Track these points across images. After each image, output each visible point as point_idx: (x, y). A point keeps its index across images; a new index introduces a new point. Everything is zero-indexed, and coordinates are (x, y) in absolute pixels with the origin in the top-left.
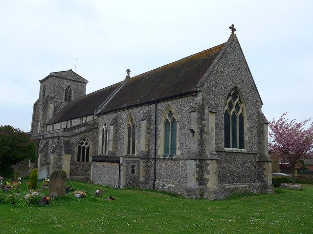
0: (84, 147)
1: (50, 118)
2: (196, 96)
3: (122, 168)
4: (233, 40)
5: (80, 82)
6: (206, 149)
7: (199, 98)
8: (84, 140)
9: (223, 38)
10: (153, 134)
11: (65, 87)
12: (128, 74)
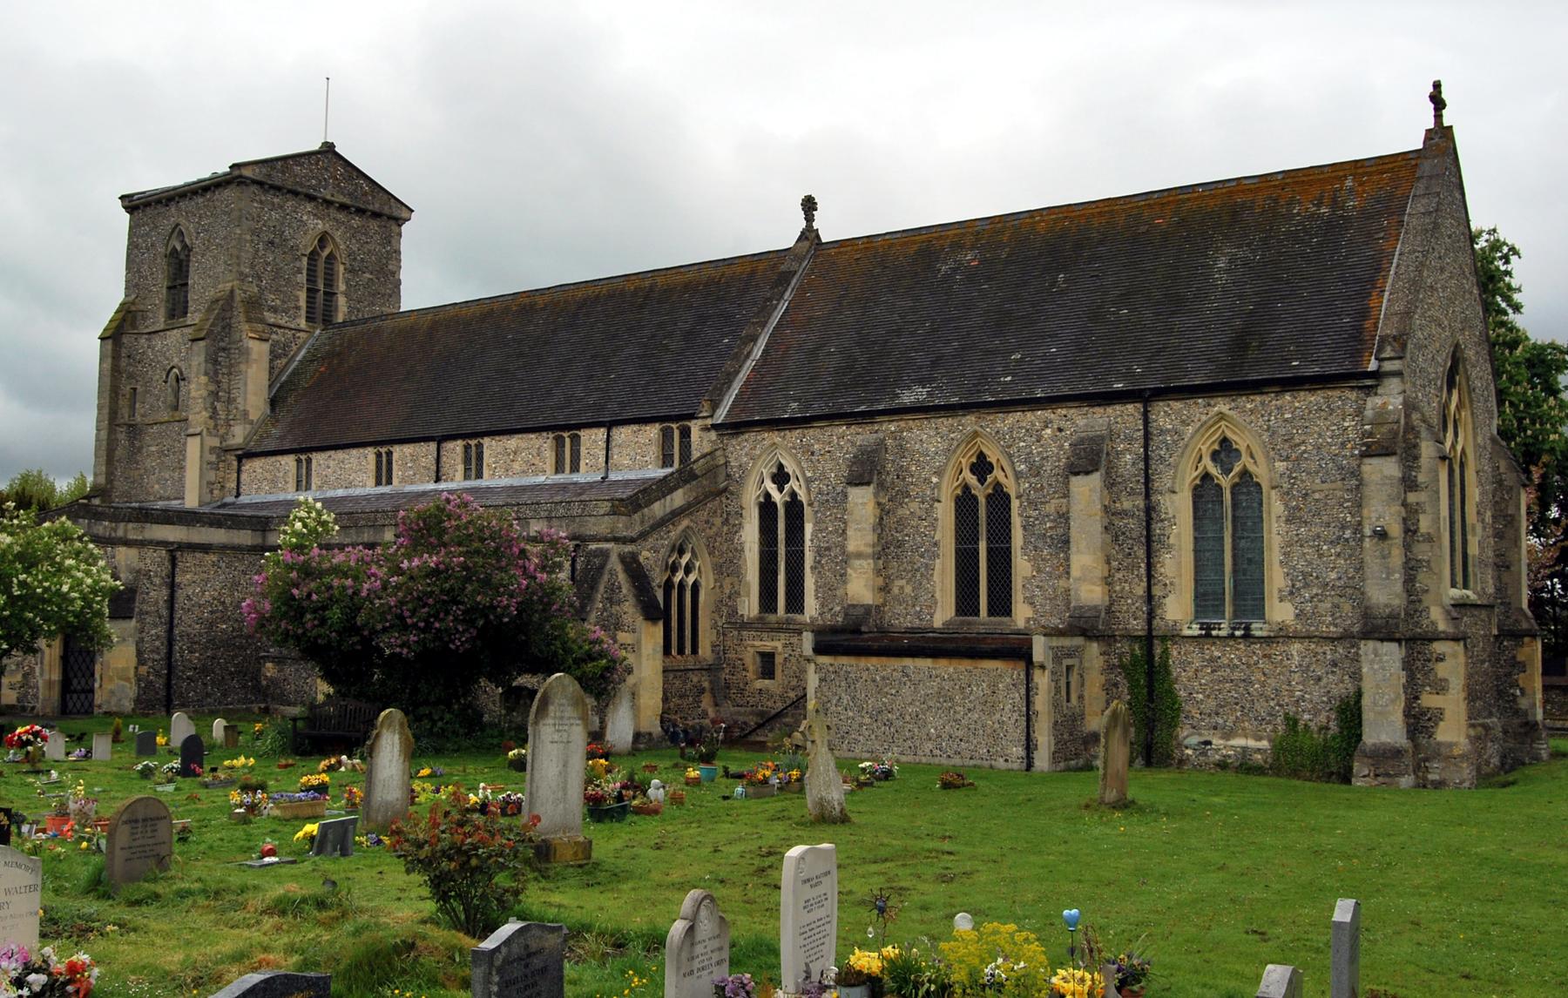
0: (682, 585)
1: (254, 415)
2: (1370, 390)
3: (1042, 680)
4: (1441, 139)
5: (376, 215)
6: (1427, 600)
7: (1390, 398)
8: (681, 552)
9: (1405, 133)
10: (1141, 538)
11: (307, 243)
12: (809, 218)
